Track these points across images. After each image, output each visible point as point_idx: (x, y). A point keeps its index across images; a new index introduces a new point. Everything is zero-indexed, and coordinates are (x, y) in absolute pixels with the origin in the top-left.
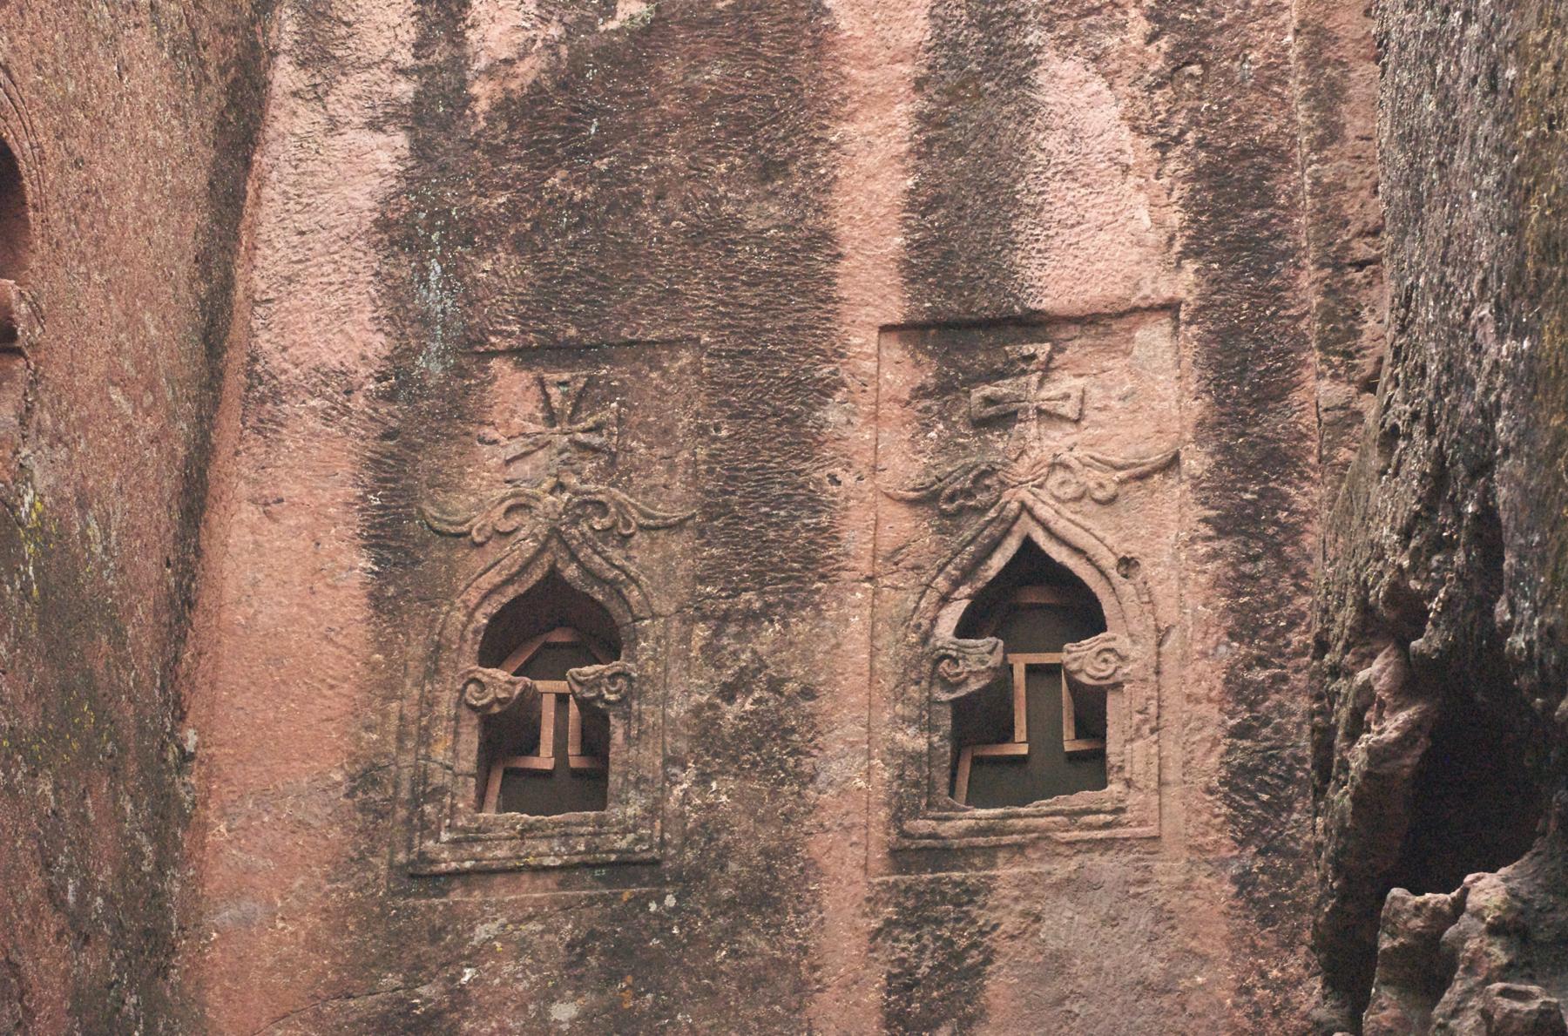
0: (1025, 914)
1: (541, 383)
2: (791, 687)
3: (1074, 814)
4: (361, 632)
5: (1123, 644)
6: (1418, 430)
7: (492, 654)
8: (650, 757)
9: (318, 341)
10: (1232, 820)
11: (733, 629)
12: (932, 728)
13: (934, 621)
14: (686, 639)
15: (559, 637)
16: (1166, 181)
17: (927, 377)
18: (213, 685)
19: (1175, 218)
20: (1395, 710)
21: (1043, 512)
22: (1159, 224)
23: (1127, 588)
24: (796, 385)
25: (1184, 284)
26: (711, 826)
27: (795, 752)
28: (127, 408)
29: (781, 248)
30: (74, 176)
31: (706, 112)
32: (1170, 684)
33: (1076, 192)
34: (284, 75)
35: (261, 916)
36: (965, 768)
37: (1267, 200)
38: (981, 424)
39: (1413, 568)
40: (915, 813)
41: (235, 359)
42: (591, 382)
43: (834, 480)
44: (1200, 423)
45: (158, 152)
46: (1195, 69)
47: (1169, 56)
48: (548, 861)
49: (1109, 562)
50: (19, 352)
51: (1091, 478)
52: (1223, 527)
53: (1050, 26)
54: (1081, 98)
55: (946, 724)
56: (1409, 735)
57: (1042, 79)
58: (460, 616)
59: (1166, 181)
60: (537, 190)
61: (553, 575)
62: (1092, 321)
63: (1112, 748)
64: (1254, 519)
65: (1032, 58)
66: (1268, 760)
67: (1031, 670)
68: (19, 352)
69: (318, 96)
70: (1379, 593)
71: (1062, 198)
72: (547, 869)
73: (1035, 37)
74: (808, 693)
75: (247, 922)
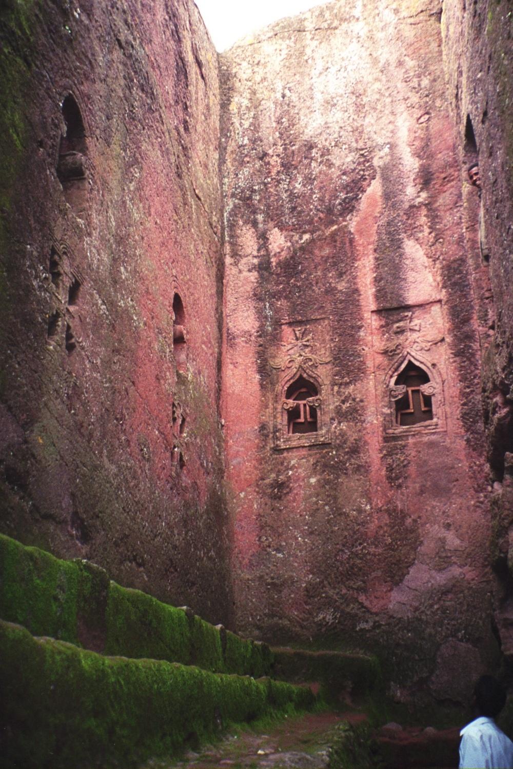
0: (416, 451)
1: (294, 331)
2: (358, 399)
3: (426, 426)
4: (259, 393)
5: (434, 385)
6: (505, 346)
7: (288, 397)
8: (327, 419)
9: (242, 324)
10: (464, 426)
11: (343, 387)
12: (390, 408)
13: (389, 382)
14: (332, 390)
15: (303, 390)
16: (435, 269)
17: (383, 323)
18: (226, 408)
19: (439, 278)
20: (503, 408)
21: (413, 354)
22: (435, 280)
23: (434, 371)
24: (353, 327)
25: (443, 295)
26: (343, 434)
27: (360, 415)
28: (205, 349)
29: (346, 294)
30: (192, 298)
31: (326, 261)
32: (446, 393)
33: (414, 274)
34: (228, 260)
35: (242, 462)
36: (399, 417)
37: (461, 272)
38: (396, 333)
39: (506, 378)
40: (389, 428)
41: (224, 330)
42: (306, 330)
43: (363, 350)
44: (449, 330)
45: (207, 287)
46: (441, 240)
47: (435, 237)
48: (306, 445)
49: (429, 365)
50: (185, 342)
51: (424, 345)
52: (456, 355)
53: (405, 232)
54: (414, 250)
55: (394, 406)
56: (507, 414)
57: (404, 246)
58: (281, 388)
59: (435, 269)
60: (289, 284)
61: (301, 377)
62: (420, 306)
63: (434, 409)
64: (463, 352)
65: (400, 241)
66: (471, 411)
67: (413, 391)
68: (185, 342)
69: (236, 264)
70: (498, 383)
71: (411, 276)
72: (306, 447)
73: (403, 235)
74: (362, 401)
75: (239, 463)
